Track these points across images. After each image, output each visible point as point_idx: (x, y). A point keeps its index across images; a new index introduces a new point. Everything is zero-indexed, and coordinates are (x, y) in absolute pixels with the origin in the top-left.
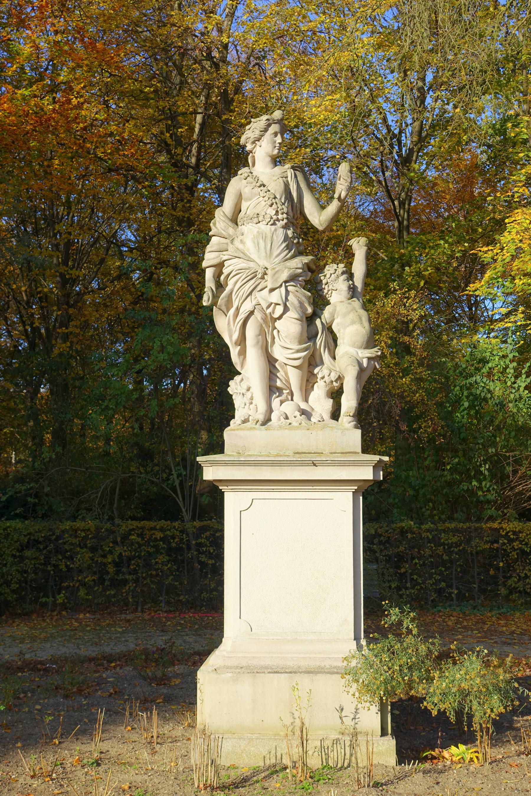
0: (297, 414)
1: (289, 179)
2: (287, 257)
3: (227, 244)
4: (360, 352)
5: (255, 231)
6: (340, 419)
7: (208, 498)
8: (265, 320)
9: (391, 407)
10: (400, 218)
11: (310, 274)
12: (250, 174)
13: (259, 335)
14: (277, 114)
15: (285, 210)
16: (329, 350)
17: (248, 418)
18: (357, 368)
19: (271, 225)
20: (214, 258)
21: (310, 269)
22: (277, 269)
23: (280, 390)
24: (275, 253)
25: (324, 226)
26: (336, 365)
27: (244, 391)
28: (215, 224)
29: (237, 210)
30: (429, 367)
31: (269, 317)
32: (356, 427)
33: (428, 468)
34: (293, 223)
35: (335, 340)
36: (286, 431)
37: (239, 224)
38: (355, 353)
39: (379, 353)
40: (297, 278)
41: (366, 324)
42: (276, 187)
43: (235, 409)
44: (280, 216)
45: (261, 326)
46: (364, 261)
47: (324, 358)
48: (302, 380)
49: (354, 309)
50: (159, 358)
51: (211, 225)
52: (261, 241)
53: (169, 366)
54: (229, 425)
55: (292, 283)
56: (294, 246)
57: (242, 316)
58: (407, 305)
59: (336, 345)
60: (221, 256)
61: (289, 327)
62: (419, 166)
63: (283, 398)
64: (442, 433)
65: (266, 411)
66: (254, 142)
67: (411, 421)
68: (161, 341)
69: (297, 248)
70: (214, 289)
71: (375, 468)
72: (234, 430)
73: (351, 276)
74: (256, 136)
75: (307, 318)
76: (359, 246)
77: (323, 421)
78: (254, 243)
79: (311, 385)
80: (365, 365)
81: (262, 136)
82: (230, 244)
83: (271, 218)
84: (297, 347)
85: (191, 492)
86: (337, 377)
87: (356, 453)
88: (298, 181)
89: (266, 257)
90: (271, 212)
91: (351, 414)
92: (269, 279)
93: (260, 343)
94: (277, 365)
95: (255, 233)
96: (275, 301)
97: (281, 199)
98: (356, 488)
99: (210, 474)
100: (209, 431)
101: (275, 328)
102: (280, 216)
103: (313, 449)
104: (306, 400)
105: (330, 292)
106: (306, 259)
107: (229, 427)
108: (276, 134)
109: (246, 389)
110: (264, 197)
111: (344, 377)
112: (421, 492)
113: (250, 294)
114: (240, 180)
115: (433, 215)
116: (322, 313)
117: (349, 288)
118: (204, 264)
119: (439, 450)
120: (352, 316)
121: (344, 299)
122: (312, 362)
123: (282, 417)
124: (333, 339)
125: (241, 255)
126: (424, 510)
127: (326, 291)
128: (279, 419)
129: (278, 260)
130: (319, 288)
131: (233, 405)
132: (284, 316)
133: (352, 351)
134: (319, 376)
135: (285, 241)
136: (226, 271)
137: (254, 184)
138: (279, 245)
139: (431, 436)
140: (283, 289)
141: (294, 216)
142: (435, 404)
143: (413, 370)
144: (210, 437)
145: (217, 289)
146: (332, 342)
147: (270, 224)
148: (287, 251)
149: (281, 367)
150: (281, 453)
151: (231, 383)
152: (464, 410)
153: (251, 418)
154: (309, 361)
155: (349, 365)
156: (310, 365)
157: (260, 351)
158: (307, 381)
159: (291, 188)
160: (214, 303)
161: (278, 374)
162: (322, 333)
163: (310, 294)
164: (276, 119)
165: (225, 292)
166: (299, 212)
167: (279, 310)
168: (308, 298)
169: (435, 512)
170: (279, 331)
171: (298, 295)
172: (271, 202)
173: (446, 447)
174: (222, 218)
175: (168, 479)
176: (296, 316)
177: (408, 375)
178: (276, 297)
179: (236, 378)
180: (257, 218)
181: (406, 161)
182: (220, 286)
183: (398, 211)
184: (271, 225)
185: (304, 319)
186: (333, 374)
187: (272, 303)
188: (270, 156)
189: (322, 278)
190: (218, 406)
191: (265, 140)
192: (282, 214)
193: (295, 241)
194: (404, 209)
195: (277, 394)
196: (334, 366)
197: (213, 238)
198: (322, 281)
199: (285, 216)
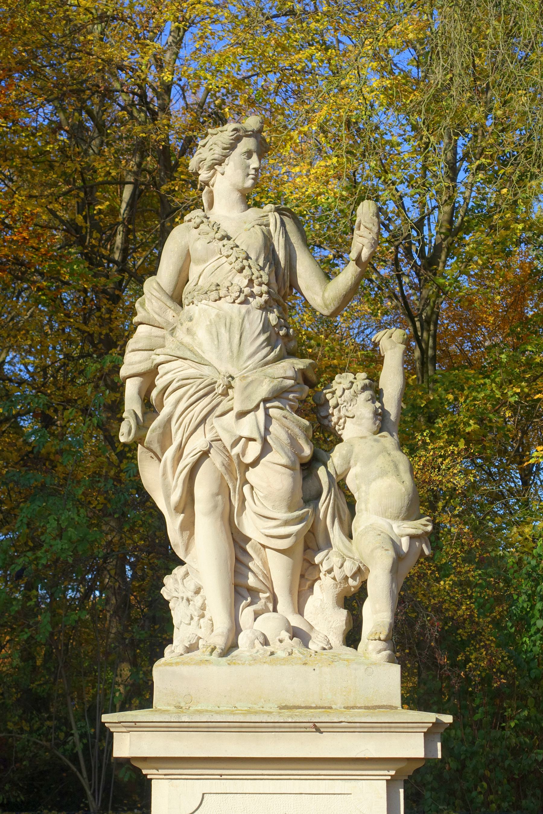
0: (285, 635)
1: (272, 228)
2: (269, 358)
3: (164, 337)
4: (395, 525)
5: (213, 313)
6: (361, 645)
7: (128, 773)
8: (228, 467)
9: (423, 626)
10: (423, 345)
11: (307, 388)
12: (205, 220)
13: (218, 494)
14: (252, 122)
15: (265, 279)
16: (341, 522)
17: (197, 643)
18: (391, 553)
19: (241, 303)
20: (140, 362)
21: (307, 381)
22: (250, 379)
23: (253, 593)
24: (248, 350)
25: (332, 308)
26: (354, 548)
27: (190, 594)
28: (143, 305)
29: (182, 279)
30: (481, 563)
31: (235, 461)
32: (391, 660)
33: (479, 724)
34: (277, 302)
35: (351, 504)
36: (266, 666)
37: (185, 302)
38: (387, 527)
39: (430, 528)
40: (285, 395)
41: (407, 477)
42: (250, 241)
43: (173, 626)
44: (256, 289)
45: (222, 478)
46: (401, 369)
47: (331, 536)
48: (293, 574)
49: (384, 450)
50: (54, 548)
51: (137, 305)
52: (223, 330)
53: (70, 560)
54: (162, 656)
55: (276, 403)
56: (280, 341)
57: (188, 460)
58: (443, 467)
59: (353, 513)
60: (153, 357)
61: (272, 479)
62: (450, 266)
63: (259, 606)
64: (503, 669)
65: (230, 630)
66: (211, 167)
67: (455, 648)
68: (58, 520)
69: (285, 345)
70: (140, 414)
71: (428, 736)
72: (170, 664)
73: (378, 395)
74: (216, 156)
75: (302, 465)
76: (392, 345)
77: (331, 648)
78: (211, 333)
79: (308, 583)
80: (405, 548)
81: (226, 156)
82: (168, 336)
83: (241, 291)
84: (284, 515)
85: (101, 761)
86: (355, 569)
87: (391, 707)
88: (286, 233)
89: (232, 357)
90: (241, 281)
91: (383, 637)
92: (235, 396)
93: (219, 509)
94: (248, 548)
95: (213, 316)
96: (246, 433)
97: (257, 260)
98: (393, 773)
99: (124, 747)
100: (134, 664)
101: (246, 482)
102: (256, 289)
103: (313, 701)
104: (300, 611)
105: (342, 421)
106: (301, 364)
107: (162, 660)
108: (249, 154)
109: (194, 591)
110: (228, 257)
111: (368, 570)
112: (470, 765)
113: (204, 420)
114: (188, 229)
115: (467, 346)
116: (329, 457)
117: (376, 414)
118: (124, 372)
119: (498, 695)
120: (381, 461)
121: (368, 434)
122: (309, 545)
123: (257, 642)
124: (348, 504)
125: (188, 355)
126: (474, 794)
127: (334, 419)
128: (253, 645)
129: (251, 363)
130: (323, 414)
131: (170, 619)
132: (263, 461)
133: (382, 523)
134: (324, 568)
135: (264, 330)
136: (160, 383)
137: (212, 234)
138: (255, 338)
139: (484, 674)
140: (261, 413)
141: (279, 291)
142: (489, 623)
143: (454, 568)
144: (133, 674)
145: (144, 414)
146: (345, 507)
147: (238, 301)
148: (268, 348)
149: (255, 551)
150: (257, 707)
151: (168, 580)
152: (536, 633)
153: (201, 642)
154: (305, 542)
155: (376, 548)
156: (307, 548)
157: (219, 523)
158: (302, 576)
159: (276, 248)
160: (139, 440)
161: (251, 565)
162: (329, 491)
163: (307, 423)
164: (249, 129)
165: (159, 418)
166: (288, 284)
167: (254, 449)
168: (305, 430)
169: (491, 797)
170: (252, 488)
171: (286, 425)
172: (240, 265)
173: (508, 691)
174: (155, 293)
175: (65, 743)
176: (284, 460)
177: (448, 576)
178: (248, 426)
179: (175, 571)
180: (216, 292)
181: (431, 263)
182: (150, 408)
183: (419, 334)
184: (241, 303)
185: (298, 467)
186: (348, 564)
187: (241, 438)
188: (239, 191)
189: (328, 396)
190: (147, 623)
191: (231, 164)
192: (260, 285)
193: (282, 333)
194: (429, 331)
195: (249, 599)
196: (350, 550)
197: (140, 328)
198: (328, 401)
199: (264, 288)
